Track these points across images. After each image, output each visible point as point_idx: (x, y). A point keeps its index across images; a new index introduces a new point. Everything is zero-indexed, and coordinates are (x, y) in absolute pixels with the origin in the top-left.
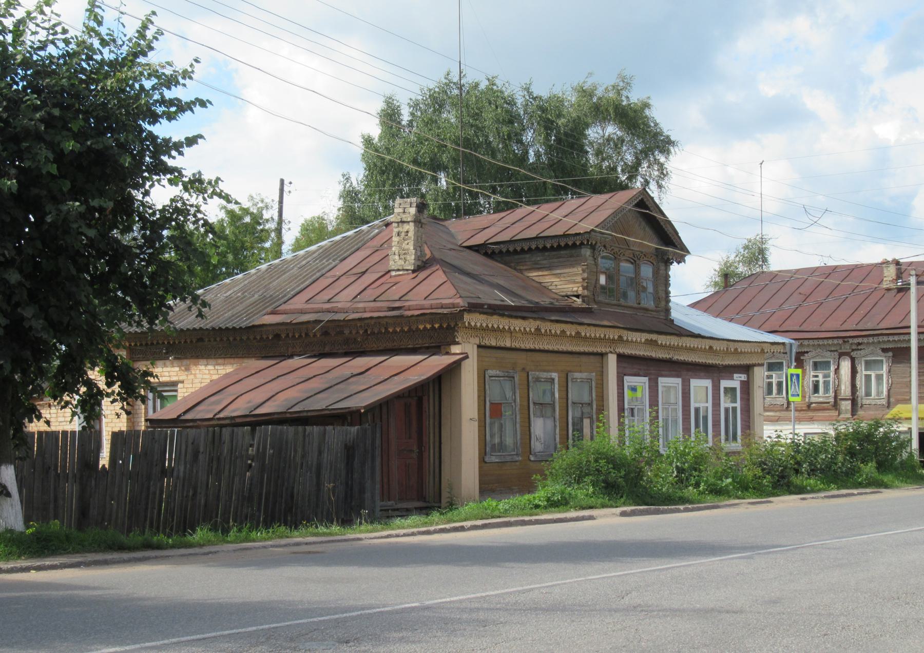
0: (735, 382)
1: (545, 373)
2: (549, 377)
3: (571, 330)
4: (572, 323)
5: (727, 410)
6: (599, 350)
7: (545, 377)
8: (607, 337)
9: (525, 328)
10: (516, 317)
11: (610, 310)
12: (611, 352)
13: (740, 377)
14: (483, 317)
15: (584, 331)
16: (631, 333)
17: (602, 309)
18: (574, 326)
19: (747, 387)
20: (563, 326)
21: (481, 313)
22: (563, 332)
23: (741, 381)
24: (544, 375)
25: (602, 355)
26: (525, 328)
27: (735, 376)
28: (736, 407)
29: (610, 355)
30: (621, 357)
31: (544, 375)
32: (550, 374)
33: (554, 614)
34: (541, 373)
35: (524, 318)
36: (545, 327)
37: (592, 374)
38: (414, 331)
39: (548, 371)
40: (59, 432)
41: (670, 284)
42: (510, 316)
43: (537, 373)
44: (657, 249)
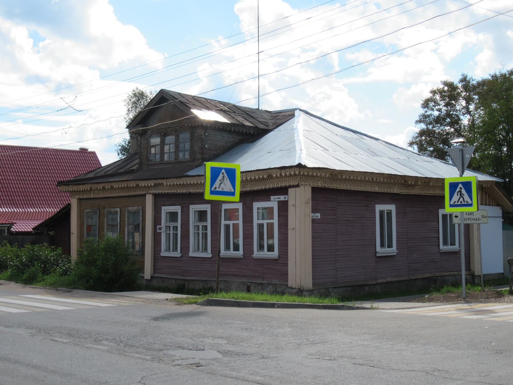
0: (273, 203)
1: (113, 209)
2: (115, 211)
3: (108, 186)
4: (107, 182)
5: (261, 226)
6: (141, 193)
7: (113, 211)
8: (129, 186)
9: (85, 189)
10: (80, 184)
11: (156, 167)
12: (147, 193)
13: (279, 198)
14: (65, 187)
15: (115, 186)
16: (150, 181)
17: (151, 168)
18: (109, 184)
19: (283, 207)
20: (103, 185)
21: (64, 185)
22: (104, 188)
23: (279, 202)
24: (113, 210)
25: (144, 195)
26: (85, 189)
27: (272, 198)
28: (272, 223)
29: (147, 195)
30: (156, 196)
31: (113, 210)
32: (116, 209)
33: (505, 349)
34: (111, 209)
35: (83, 184)
36: (94, 187)
37: (140, 207)
38: (297, 175)
39: (114, 208)
40: (447, 214)
41: (94, 153)
42: (77, 185)
43: (109, 209)
44: (189, 115)
